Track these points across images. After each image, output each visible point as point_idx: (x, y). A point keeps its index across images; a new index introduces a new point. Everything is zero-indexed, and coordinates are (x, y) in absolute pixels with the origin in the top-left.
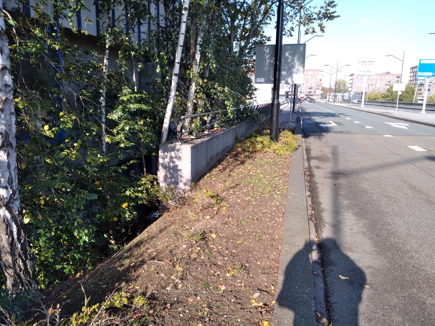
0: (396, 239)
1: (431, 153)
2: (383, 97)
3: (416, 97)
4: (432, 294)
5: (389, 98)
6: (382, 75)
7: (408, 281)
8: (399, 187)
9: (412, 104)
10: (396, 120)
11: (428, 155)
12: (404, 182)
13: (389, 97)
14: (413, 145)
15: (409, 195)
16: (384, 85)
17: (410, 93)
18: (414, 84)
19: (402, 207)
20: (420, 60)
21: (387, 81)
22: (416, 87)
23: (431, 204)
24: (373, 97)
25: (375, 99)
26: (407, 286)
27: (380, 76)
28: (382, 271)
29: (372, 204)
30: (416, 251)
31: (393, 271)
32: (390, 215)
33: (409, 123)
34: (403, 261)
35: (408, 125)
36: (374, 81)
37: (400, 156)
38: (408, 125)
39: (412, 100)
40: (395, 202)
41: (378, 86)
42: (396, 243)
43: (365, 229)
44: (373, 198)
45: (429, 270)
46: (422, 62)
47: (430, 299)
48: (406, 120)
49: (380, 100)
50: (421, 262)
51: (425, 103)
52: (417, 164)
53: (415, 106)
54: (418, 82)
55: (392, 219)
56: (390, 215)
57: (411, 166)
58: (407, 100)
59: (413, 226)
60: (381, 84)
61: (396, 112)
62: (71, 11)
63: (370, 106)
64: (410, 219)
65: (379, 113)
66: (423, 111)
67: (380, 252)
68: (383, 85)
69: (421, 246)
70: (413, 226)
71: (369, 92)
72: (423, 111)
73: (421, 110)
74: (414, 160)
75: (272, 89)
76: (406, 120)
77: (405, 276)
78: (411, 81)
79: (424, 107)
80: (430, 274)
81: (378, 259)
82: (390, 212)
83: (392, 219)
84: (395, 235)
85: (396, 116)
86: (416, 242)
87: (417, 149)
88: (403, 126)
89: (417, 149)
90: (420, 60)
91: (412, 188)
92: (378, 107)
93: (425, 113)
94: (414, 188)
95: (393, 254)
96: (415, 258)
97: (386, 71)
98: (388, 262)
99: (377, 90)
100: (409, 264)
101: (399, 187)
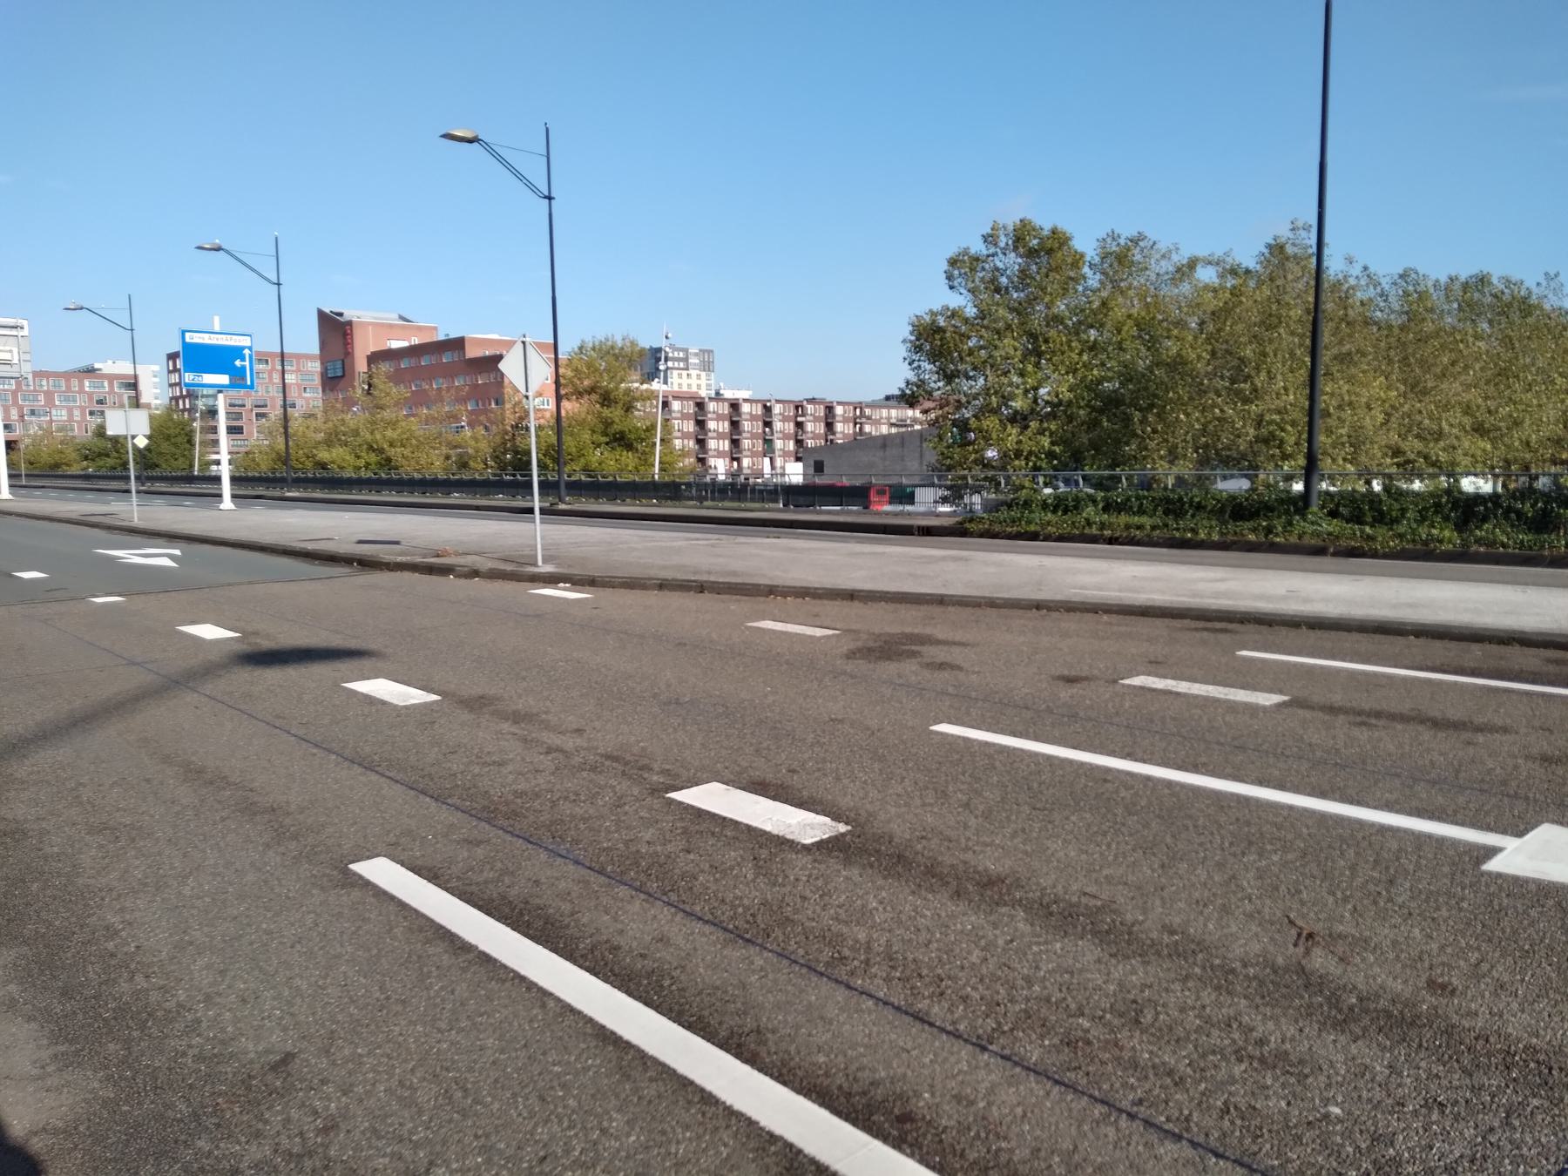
0: (139, 978)
1: (253, 640)
2: (86, 458)
3: (201, 455)
4: (260, 1126)
5: (110, 462)
6: (68, 375)
7: (180, 1121)
8: (148, 781)
9: (191, 479)
10: (138, 539)
11: (245, 648)
12: (167, 760)
13: (107, 456)
14: (193, 622)
15: (184, 801)
16: (83, 414)
17: (179, 439)
18: (189, 410)
19: (159, 854)
20: (183, 332)
21: (91, 398)
22: (195, 420)
23: (255, 814)
24: (45, 458)
25: (57, 466)
26: (176, 1142)
27: (63, 382)
28: (81, 1128)
29: (42, 873)
30: (208, 999)
31: (126, 1108)
32: (114, 894)
33: (184, 545)
34: (161, 1052)
35: (177, 552)
36: (41, 397)
37: (149, 666)
38: (177, 552)
39: (192, 466)
40: (133, 840)
41: (60, 415)
42: (136, 994)
43: (12, 988)
44: (48, 850)
45: (251, 1047)
46: (189, 338)
47: (254, 1148)
48: (171, 537)
49: (75, 469)
50: (223, 1030)
51: (225, 471)
52: (208, 688)
53: (202, 485)
54: (201, 404)
55: (122, 910)
56: (114, 894)
57: (191, 698)
58: (170, 464)
59: (195, 912)
60: (70, 410)
61: (133, 509)
62: (651, 1080)
63: (38, 493)
64: (187, 891)
65: (73, 516)
66: (227, 503)
67: (77, 1053)
68: (77, 413)
69: (222, 973)
70: (195, 912)
71: (27, 441)
72: (227, 503)
73: (220, 496)
74: (207, 668)
75: (1483, 280)
76: (171, 537)
77: (167, 1106)
78: (176, 399)
79: (226, 487)
80: (251, 1062)
81: (68, 1084)
82: (115, 883)
83: (122, 910)
84: (133, 966)
85: (136, 522)
86: (208, 967)
87: (208, 632)
88: (161, 558)
89: (208, 632)
90: (183, 332)
91: (193, 773)
92: (71, 495)
93: (232, 506)
94: (200, 771)
95: (128, 1043)
96: (204, 1025)
97: (83, 363)
98: (108, 1078)
99: (59, 430)
100: (184, 1054)
101: (148, 781)
